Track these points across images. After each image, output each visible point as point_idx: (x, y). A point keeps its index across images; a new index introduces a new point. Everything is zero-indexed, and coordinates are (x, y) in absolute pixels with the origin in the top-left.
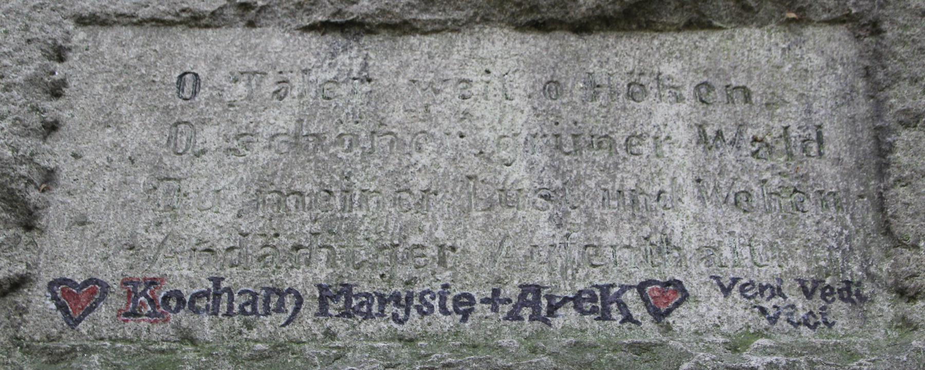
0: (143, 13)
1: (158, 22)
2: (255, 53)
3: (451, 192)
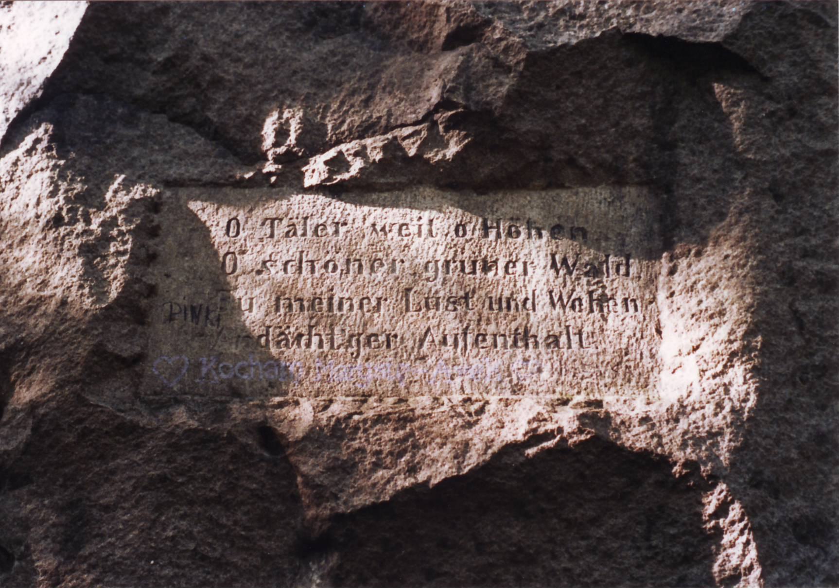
0: (207, 177)
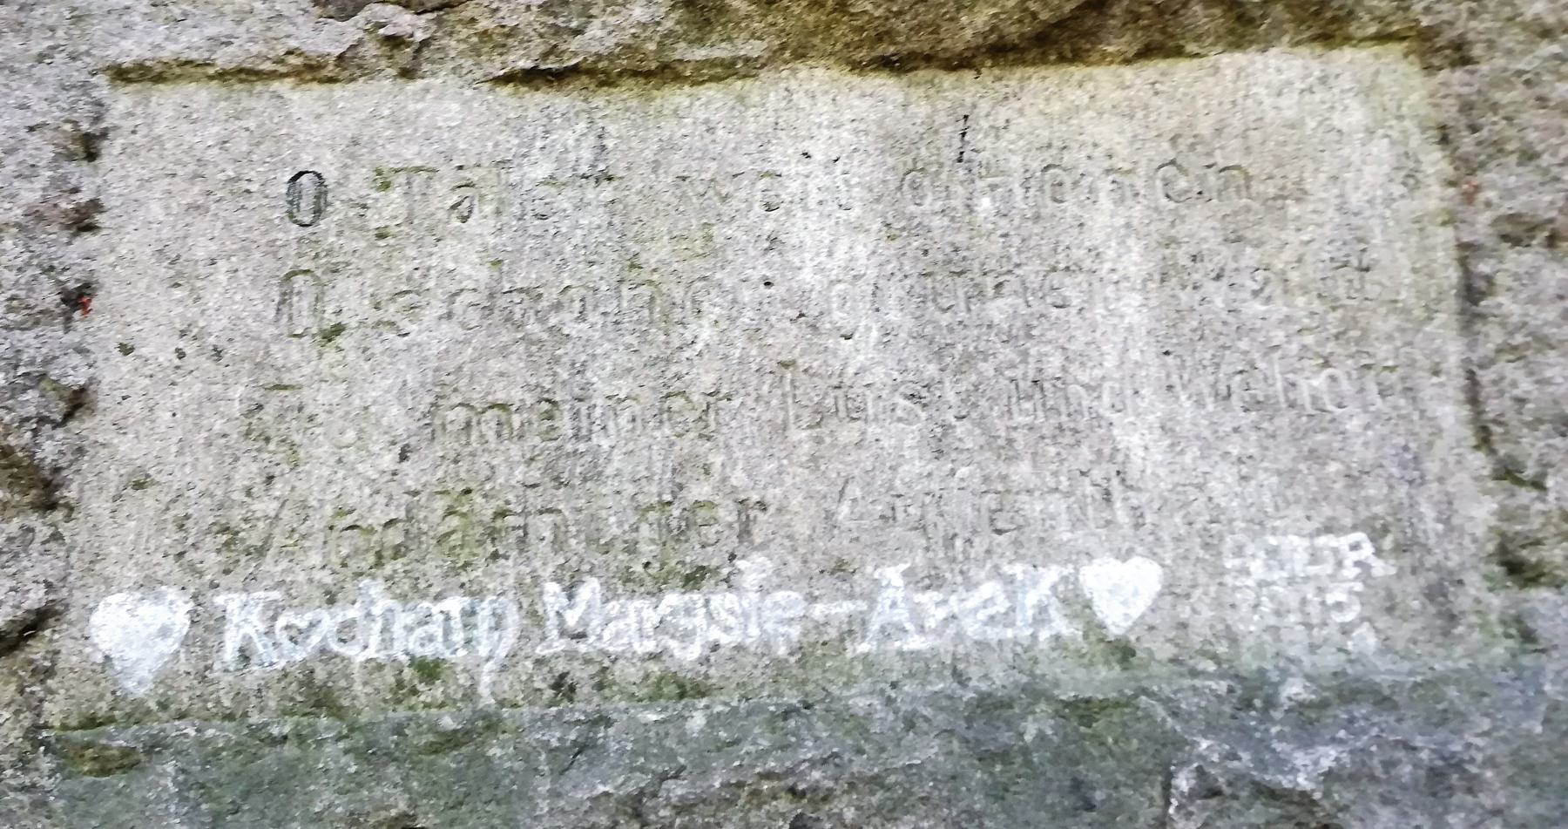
0: (224, 58)
1: (246, 74)
2: (416, 130)
3: (754, 395)
